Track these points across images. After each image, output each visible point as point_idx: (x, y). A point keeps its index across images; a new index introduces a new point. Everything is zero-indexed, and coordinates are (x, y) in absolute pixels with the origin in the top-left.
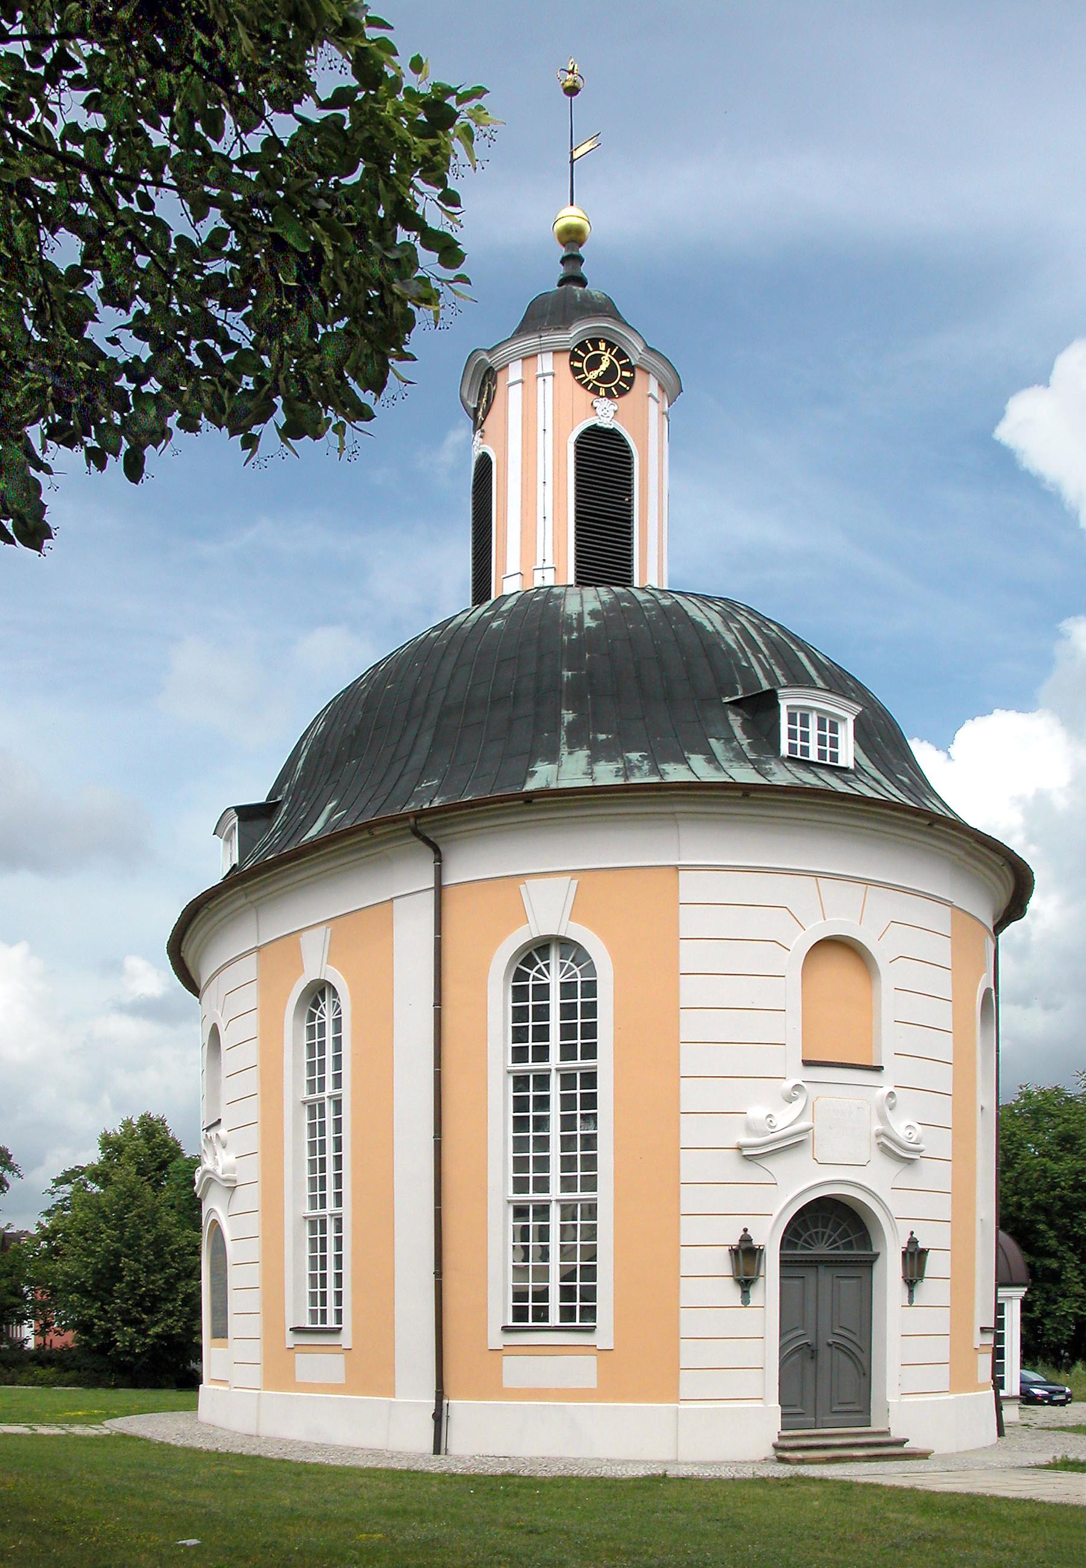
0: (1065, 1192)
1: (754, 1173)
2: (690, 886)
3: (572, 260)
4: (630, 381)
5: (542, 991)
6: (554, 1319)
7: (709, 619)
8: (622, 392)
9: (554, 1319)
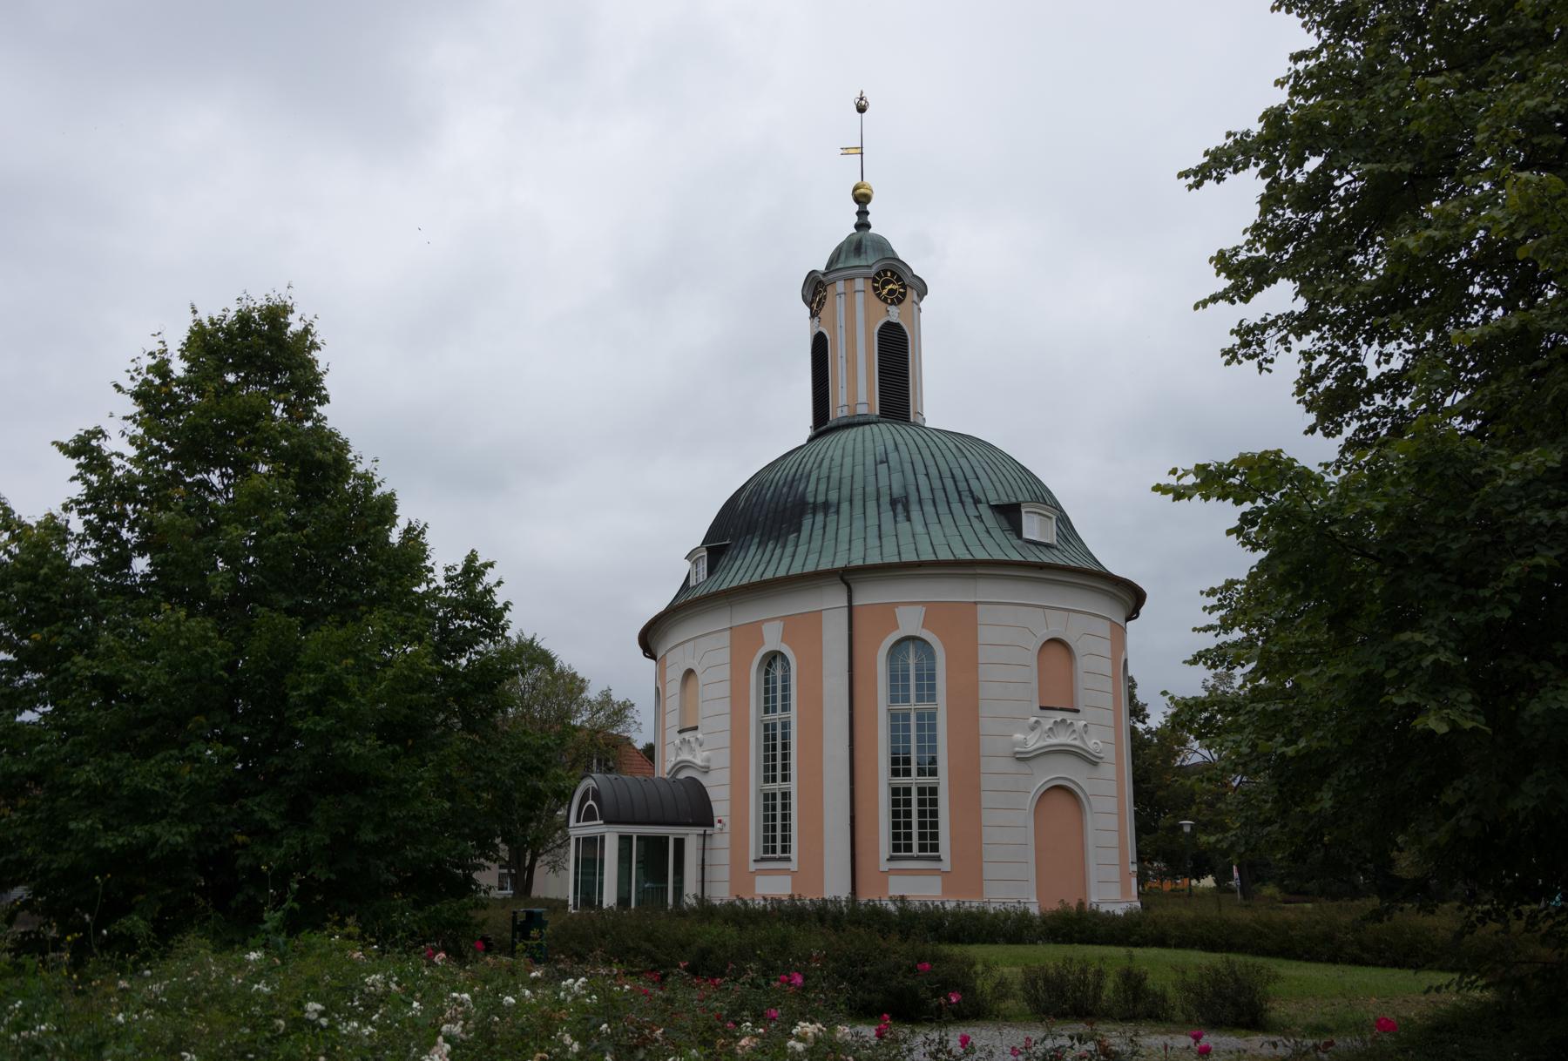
1: (1023, 768)
2: (983, 613)
3: (863, 213)
4: (904, 295)
6: (915, 852)
8: (900, 301)
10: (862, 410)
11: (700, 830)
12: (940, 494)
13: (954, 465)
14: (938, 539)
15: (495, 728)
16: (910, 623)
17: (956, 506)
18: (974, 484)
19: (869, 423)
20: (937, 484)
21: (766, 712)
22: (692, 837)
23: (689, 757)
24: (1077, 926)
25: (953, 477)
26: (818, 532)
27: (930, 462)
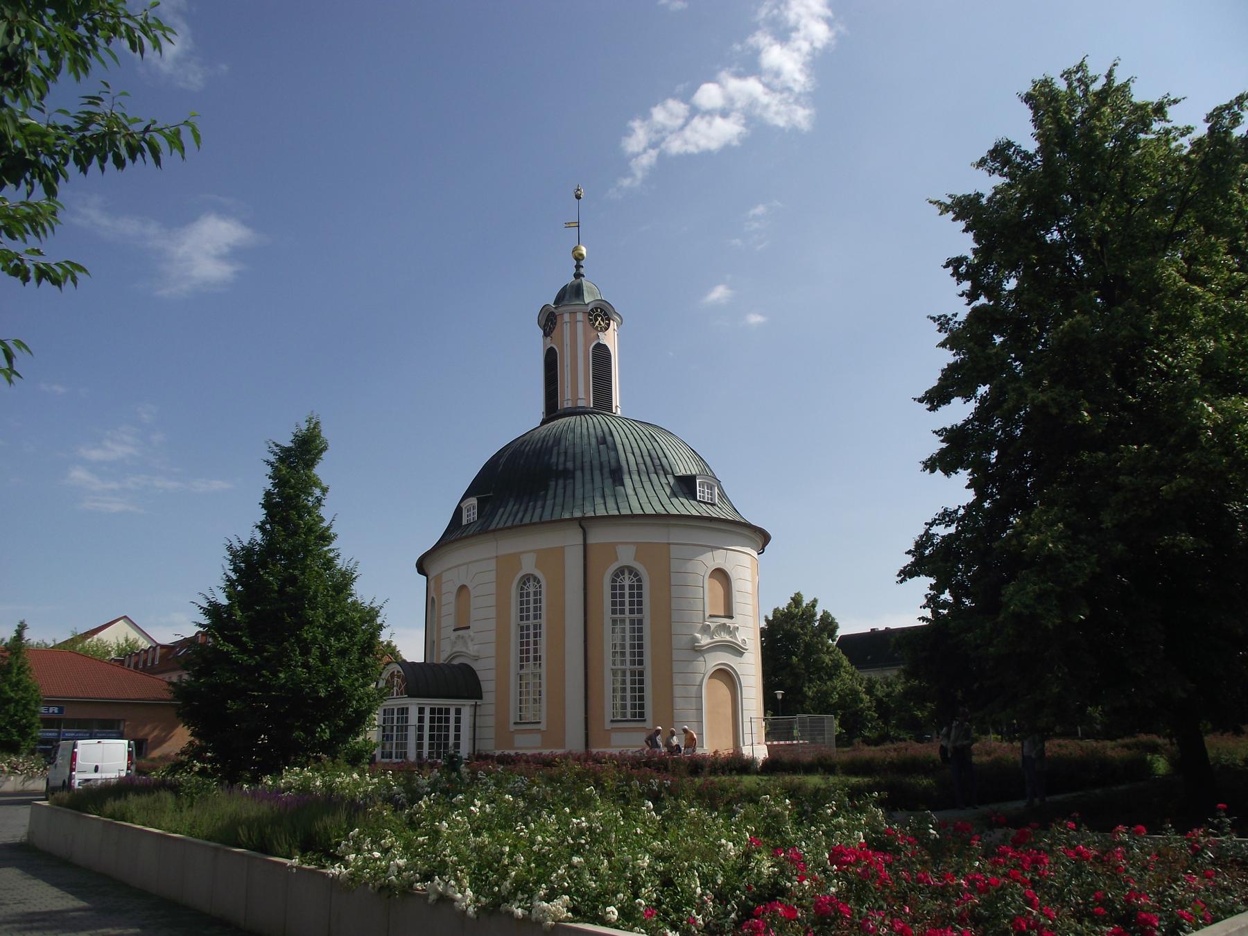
0: (866, 698)
5: (622, 587)
7: (941, 531)
9: (629, 717)
10: (581, 403)
11: (472, 702)
12: (642, 467)
13: (650, 447)
14: (644, 500)
15: (638, 810)
16: (626, 557)
17: (653, 476)
18: (664, 460)
19: (584, 413)
20: (640, 460)
21: (522, 619)
22: (467, 707)
23: (464, 649)
24: (738, 765)
25: (650, 455)
26: (560, 491)
27: (634, 445)
